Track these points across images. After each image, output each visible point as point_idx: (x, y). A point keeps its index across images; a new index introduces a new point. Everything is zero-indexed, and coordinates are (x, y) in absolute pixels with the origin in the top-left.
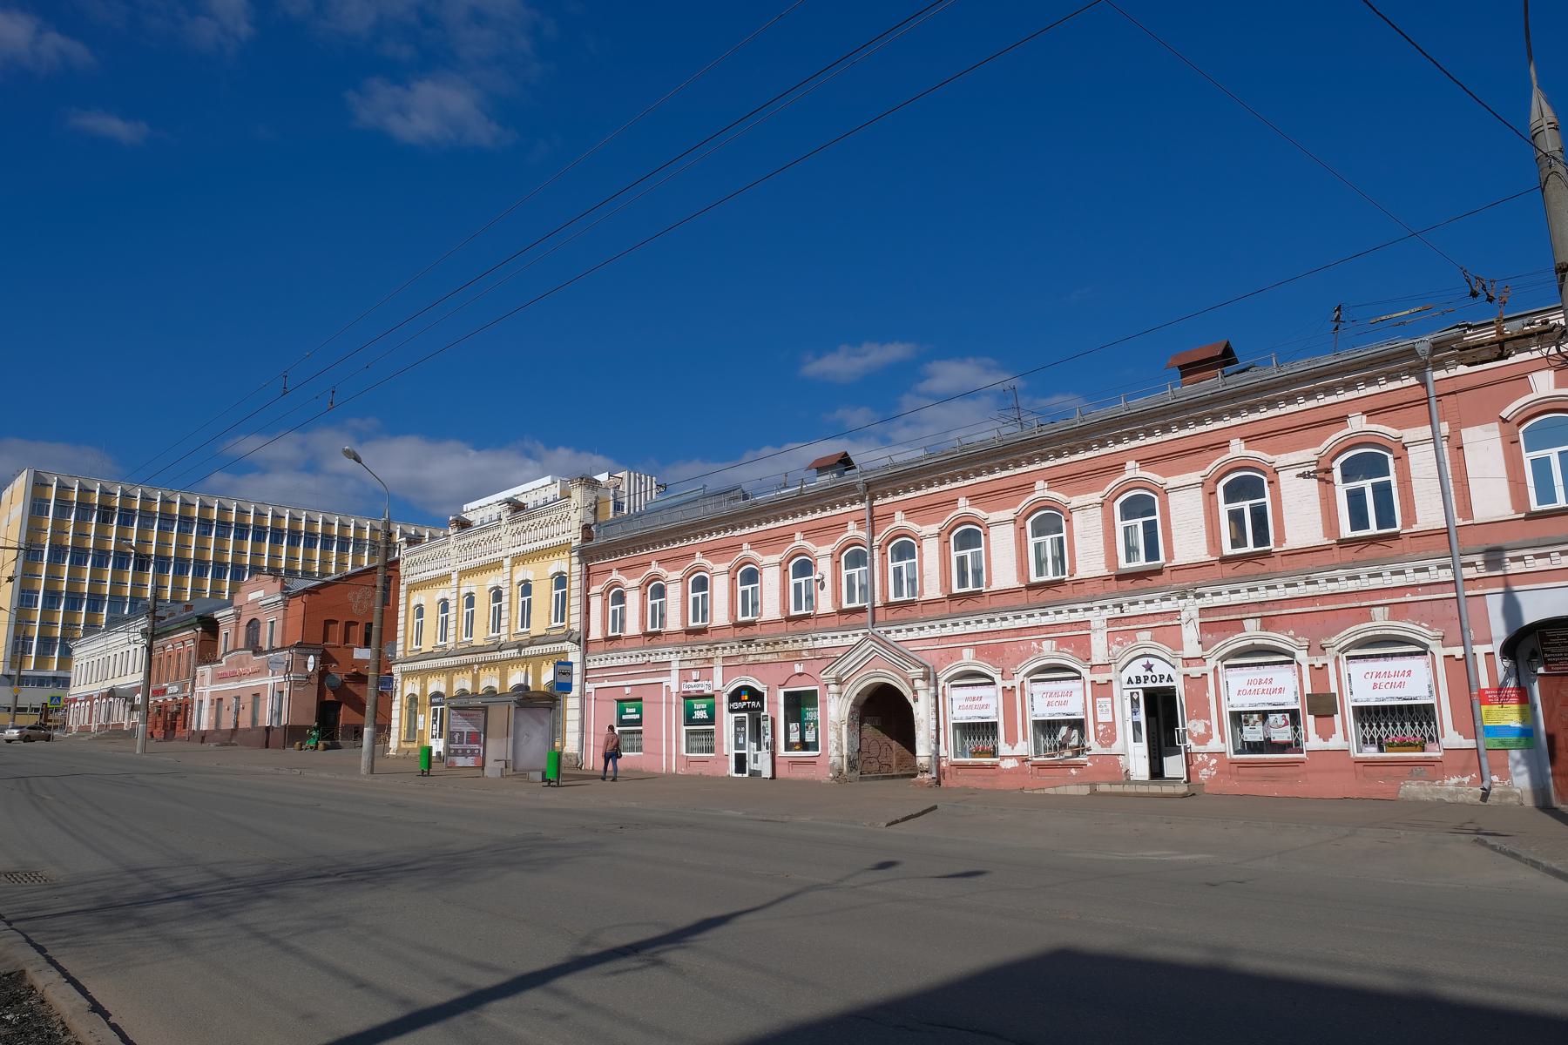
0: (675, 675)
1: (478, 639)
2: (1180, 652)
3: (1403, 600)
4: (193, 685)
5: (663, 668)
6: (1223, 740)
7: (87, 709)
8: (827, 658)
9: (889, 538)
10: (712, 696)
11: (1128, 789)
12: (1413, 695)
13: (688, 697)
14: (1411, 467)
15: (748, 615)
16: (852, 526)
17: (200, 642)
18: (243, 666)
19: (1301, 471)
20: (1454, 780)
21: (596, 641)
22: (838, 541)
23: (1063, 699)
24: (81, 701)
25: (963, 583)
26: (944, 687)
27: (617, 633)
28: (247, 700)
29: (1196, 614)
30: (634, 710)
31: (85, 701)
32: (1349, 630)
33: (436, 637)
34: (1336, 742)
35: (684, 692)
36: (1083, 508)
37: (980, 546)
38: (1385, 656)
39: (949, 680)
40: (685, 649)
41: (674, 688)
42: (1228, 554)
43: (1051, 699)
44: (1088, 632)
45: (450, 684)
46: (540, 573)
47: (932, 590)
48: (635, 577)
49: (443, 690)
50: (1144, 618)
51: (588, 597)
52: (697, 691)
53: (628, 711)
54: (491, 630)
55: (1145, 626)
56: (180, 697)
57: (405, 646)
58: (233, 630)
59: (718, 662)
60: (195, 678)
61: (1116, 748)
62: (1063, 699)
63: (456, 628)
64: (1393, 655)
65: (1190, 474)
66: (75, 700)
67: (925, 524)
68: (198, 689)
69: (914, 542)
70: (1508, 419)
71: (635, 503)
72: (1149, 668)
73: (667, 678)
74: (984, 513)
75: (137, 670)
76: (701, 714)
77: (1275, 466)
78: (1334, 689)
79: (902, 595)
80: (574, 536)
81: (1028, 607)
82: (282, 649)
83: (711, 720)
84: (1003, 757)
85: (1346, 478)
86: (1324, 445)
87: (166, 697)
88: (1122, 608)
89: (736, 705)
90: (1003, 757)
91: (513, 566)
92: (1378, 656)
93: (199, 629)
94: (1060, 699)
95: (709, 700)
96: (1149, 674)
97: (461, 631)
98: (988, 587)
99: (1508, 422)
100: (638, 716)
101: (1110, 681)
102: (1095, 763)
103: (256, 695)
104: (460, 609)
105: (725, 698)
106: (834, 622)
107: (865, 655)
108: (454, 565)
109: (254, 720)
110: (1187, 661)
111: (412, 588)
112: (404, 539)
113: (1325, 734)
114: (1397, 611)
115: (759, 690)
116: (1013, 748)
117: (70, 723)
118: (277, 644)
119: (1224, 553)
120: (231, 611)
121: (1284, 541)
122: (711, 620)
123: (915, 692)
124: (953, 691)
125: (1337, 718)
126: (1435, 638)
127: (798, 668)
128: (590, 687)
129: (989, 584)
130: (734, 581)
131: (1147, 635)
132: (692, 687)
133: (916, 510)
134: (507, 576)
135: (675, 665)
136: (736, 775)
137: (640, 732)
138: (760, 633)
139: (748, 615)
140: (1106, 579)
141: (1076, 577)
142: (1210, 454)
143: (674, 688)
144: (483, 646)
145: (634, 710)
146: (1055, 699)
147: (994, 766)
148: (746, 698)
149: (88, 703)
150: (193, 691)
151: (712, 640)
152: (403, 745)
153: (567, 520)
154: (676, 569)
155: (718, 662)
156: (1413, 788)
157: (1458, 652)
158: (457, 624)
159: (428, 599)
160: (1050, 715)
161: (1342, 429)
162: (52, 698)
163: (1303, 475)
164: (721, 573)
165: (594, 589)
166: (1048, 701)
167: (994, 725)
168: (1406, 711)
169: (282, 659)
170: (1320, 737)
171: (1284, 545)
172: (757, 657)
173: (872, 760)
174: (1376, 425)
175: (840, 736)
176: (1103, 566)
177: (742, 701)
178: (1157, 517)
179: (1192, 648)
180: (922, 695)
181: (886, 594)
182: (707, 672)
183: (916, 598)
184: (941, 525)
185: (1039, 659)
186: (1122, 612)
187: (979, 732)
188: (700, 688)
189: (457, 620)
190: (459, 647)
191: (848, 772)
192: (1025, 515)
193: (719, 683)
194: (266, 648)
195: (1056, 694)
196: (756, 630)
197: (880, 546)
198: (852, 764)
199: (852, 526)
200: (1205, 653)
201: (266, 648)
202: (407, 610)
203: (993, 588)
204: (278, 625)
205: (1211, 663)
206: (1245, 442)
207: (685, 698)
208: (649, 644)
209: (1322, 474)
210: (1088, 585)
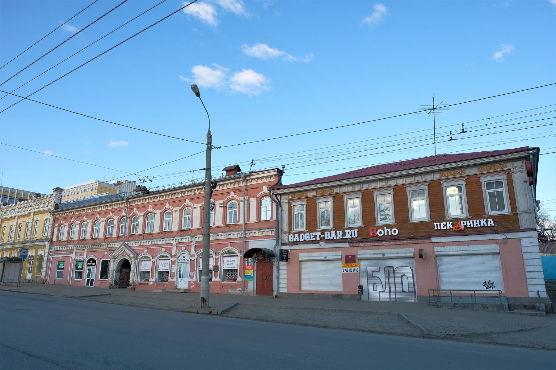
0: (74, 254)
1: (21, 239)
3: (234, 242)
5: (71, 252)
8: (113, 250)
9: (121, 217)
11: (177, 291)
13: (77, 261)
21: (55, 242)
23: (232, 263)
25: (133, 232)
26: (139, 261)
30: (62, 265)
32: (223, 249)
33: (25, 235)
35: (76, 259)
39: (141, 258)
40: (78, 246)
43: (228, 263)
44: (172, 246)
51: (54, 228)
53: (61, 265)
54: (34, 235)
59: (86, 250)
61: (174, 279)
62: (232, 263)
63: (15, 235)
64: (232, 256)
71: (125, 189)
73: (72, 255)
76: (80, 267)
81: (161, 238)
89: (89, 264)
92: (229, 256)
94: (231, 262)
95: (82, 262)
96: (184, 259)
97: (17, 236)
100: (63, 267)
101: (175, 260)
104: (17, 229)
105: (86, 262)
106: (116, 240)
114: (233, 245)
115: (95, 260)
119: (276, 220)
125: (219, 272)
128: (51, 257)
129: (153, 231)
132: (78, 258)
134: (32, 219)
135: (75, 251)
136: (86, 286)
137: (63, 272)
138: (98, 242)
140: (178, 232)
143: (73, 258)
144: (22, 242)
145: (62, 265)
146: (230, 262)
147: (148, 284)
148: (92, 262)
151: (85, 243)
153: (51, 201)
155: (86, 250)
164: (90, 223)
165: (56, 225)
166: (164, 265)
168: (143, 272)
172: (96, 249)
173: (124, 282)
177: (90, 263)
179: (193, 252)
180: (133, 263)
181: (130, 232)
182: (82, 255)
187: (145, 275)
188: (80, 258)
189: (15, 233)
193: (85, 257)
195: (230, 261)
196: (96, 241)
203: (154, 232)
205: (196, 256)
209: (224, 207)
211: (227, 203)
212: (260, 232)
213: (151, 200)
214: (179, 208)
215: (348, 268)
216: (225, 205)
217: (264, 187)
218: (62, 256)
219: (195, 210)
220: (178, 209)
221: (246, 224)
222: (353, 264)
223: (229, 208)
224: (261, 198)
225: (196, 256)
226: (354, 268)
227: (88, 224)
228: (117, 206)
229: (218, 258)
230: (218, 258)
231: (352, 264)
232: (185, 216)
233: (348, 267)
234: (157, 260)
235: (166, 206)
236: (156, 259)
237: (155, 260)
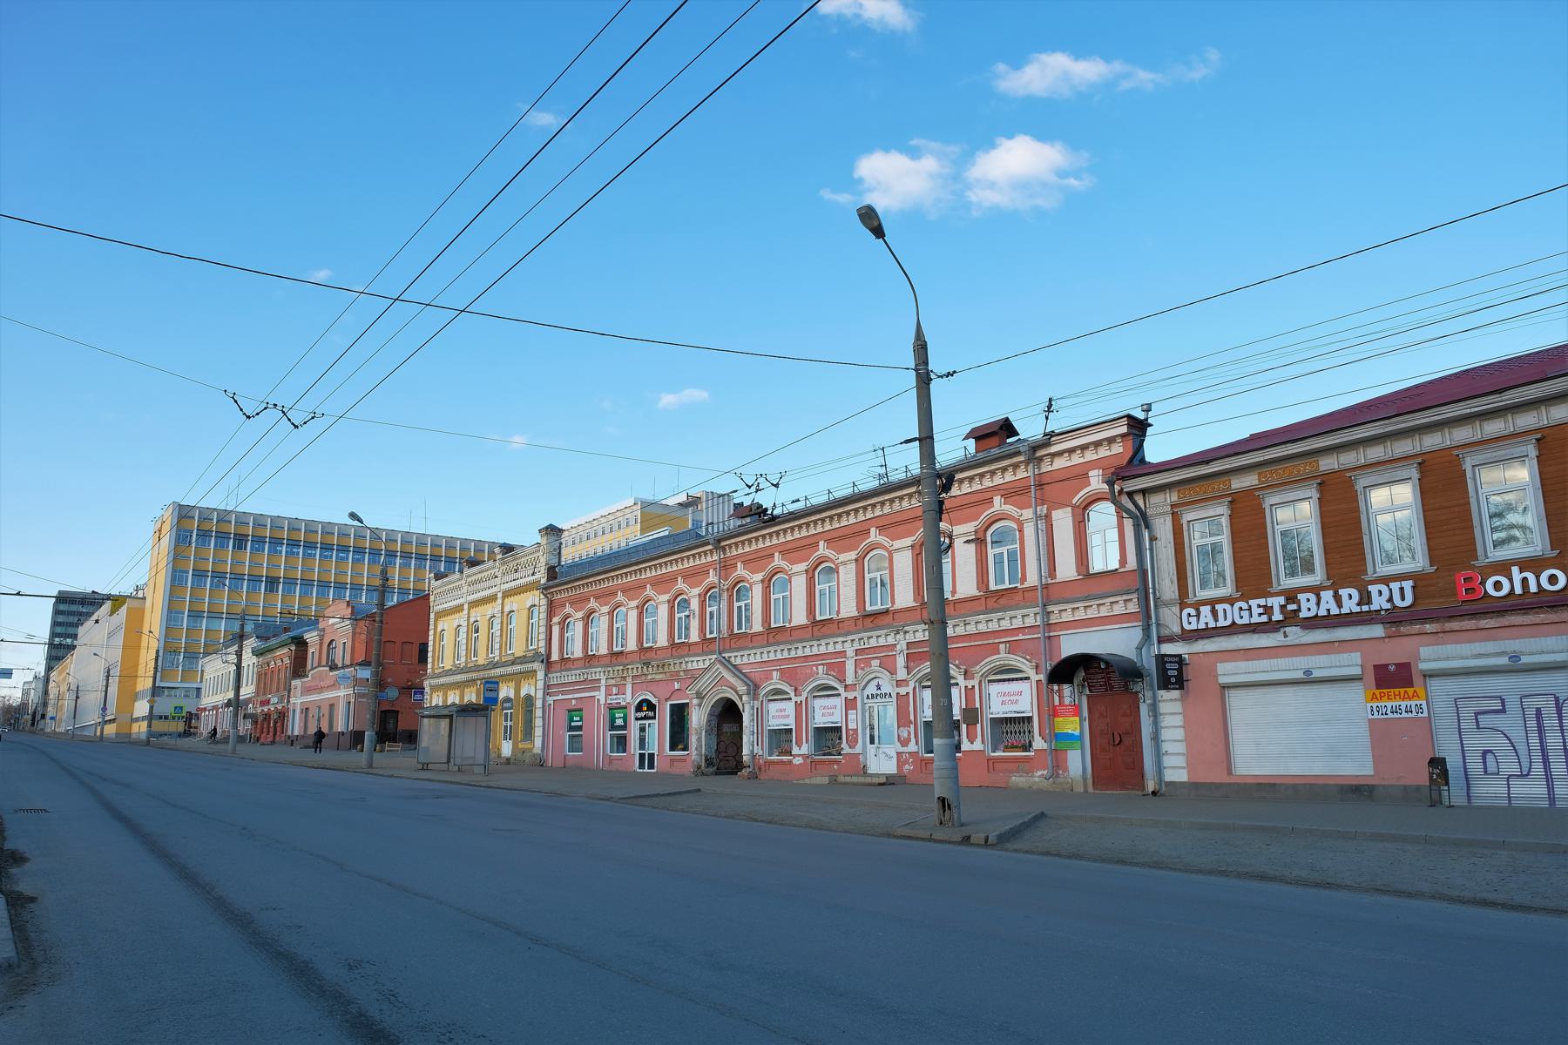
1: (481, 660)
3: (1016, 638)
4: (289, 697)
5: (594, 685)
6: (917, 743)
7: (214, 717)
8: (694, 676)
10: (625, 707)
12: (1022, 710)
17: (295, 659)
18: (323, 681)
20: (1039, 773)
24: (209, 711)
25: (740, 627)
27: (683, 640)
28: (325, 711)
29: (905, 647)
31: (212, 710)
32: (983, 663)
34: (978, 745)
38: (1009, 680)
39: (766, 695)
41: (602, 701)
45: (462, 697)
46: (518, 603)
49: (512, 695)
50: (877, 649)
51: (551, 626)
52: (617, 703)
53: (575, 719)
55: (875, 655)
56: (280, 707)
57: (433, 665)
58: (350, 638)
59: (629, 679)
60: (290, 691)
64: (1013, 680)
66: (205, 709)
67: (841, 553)
68: (292, 700)
72: (879, 687)
75: (250, 682)
76: (619, 722)
79: (1003, 582)
80: (541, 576)
82: (351, 665)
83: (624, 727)
84: (795, 756)
87: (269, 707)
90: (795, 756)
91: (469, 610)
92: (1004, 680)
93: (293, 648)
94: (1012, 698)
96: (879, 692)
97: (471, 653)
102: (846, 761)
103: (332, 706)
104: (470, 635)
106: (698, 649)
108: (500, 586)
109: (331, 726)
110: (899, 683)
111: (440, 615)
112: (433, 575)
117: (202, 729)
118: (348, 662)
120: (316, 633)
124: (990, 687)
125: (979, 726)
127: (677, 686)
128: (550, 700)
132: (613, 700)
135: (603, 682)
136: (638, 770)
137: (581, 735)
140: (855, 619)
142: (857, 538)
143: (602, 701)
148: (645, 709)
149: (215, 712)
150: (289, 701)
152: (520, 746)
155: (629, 679)
156: (1018, 780)
158: (467, 646)
159: (447, 624)
160: (1004, 713)
162: (176, 708)
163: (968, 542)
166: (827, 712)
169: (348, 675)
175: (699, 740)
183: (1018, 585)
185: (815, 680)
190: (503, 660)
191: (706, 768)
192: (984, 527)
193: (629, 698)
194: (340, 665)
197: (728, 589)
198: (709, 762)
201: (340, 665)
202: (435, 634)
204: (349, 645)
205: (912, 684)
206: (1005, 498)
207: (610, 709)
208: (996, 606)
210: (847, 623)
215: (1389, 705)
216: (980, 535)
218: (576, 696)
222: (1405, 692)
223: (992, 543)
225: (912, 684)
226: (1408, 703)
229: (973, 687)
230: (973, 687)
231: (1402, 690)
233: (1389, 699)
234: (807, 698)
236: (804, 695)
237: (803, 698)
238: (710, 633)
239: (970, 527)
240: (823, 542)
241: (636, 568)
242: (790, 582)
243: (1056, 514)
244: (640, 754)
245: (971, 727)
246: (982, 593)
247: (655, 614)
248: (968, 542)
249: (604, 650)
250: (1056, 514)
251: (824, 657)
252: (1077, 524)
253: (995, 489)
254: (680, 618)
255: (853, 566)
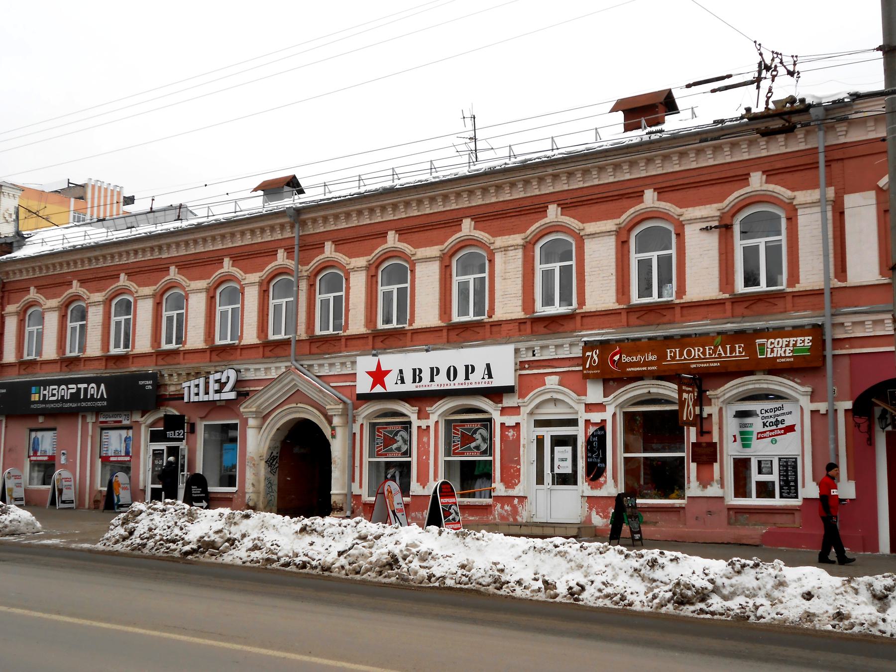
2: (583, 398)
6: (361, 486)
14: (799, 229)
15: (171, 343)
16: (281, 254)
19: (704, 225)
22: (267, 269)
26: (362, 425)
34: (713, 491)
36: (506, 249)
37: (671, 249)
42: (741, 291)
47: (357, 325)
48: (54, 297)
65: (605, 222)
69: (407, 266)
70: (884, 188)
74: (412, 249)
77: (681, 219)
78: (716, 439)
85: (744, 234)
86: (727, 202)
88: (534, 351)
98: (411, 325)
99: (884, 191)
107: (286, 389)
110: (590, 407)
113: (704, 482)
116: (424, 488)
121: (684, 293)
122: (133, 347)
123: (333, 429)
125: (716, 466)
126: (804, 394)
129: (412, 321)
130: (374, 278)
131: (555, 379)
133: (674, 188)
139: (226, 339)
140: (521, 322)
141: (495, 318)
154: (98, 291)
157: (822, 407)
161: (745, 186)
163: (706, 229)
164: (51, 309)
167: (758, 461)
170: (700, 484)
171: (797, 285)
174: (633, 208)
176: (520, 309)
178: (573, 263)
180: (339, 431)
184: (370, 258)
186: (534, 355)
199: (281, 254)
200: (606, 399)
203: (416, 325)
205: (610, 410)
209: (725, 228)
211: (377, 267)
212: (863, 323)
213: (152, 255)
214: (517, 239)
216: (727, 221)
217: (279, 251)
219: (590, 246)
220: (514, 243)
221: (833, 290)
224: (819, 202)
225: (610, 410)
227: (136, 301)
228: (152, 255)
229: (428, 427)
230: (428, 427)
232: (170, 313)
234: (437, 422)
235: (461, 230)
236: (434, 418)
237: (431, 422)
238: (70, 352)
239: (711, 210)
240: (76, 281)
241: (156, 243)
242: (243, 294)
243: (851, 201)
244: (153, 489)
245: (705, 469)
246: (370, 332)
247: (41, 320)
248: (706, 229)
249: (250, 336)
250: (851, 201)
251: (555, 363)
252: (370, 277)
253: (649, 181)
254: (31, 333)
255: (519, 253)
